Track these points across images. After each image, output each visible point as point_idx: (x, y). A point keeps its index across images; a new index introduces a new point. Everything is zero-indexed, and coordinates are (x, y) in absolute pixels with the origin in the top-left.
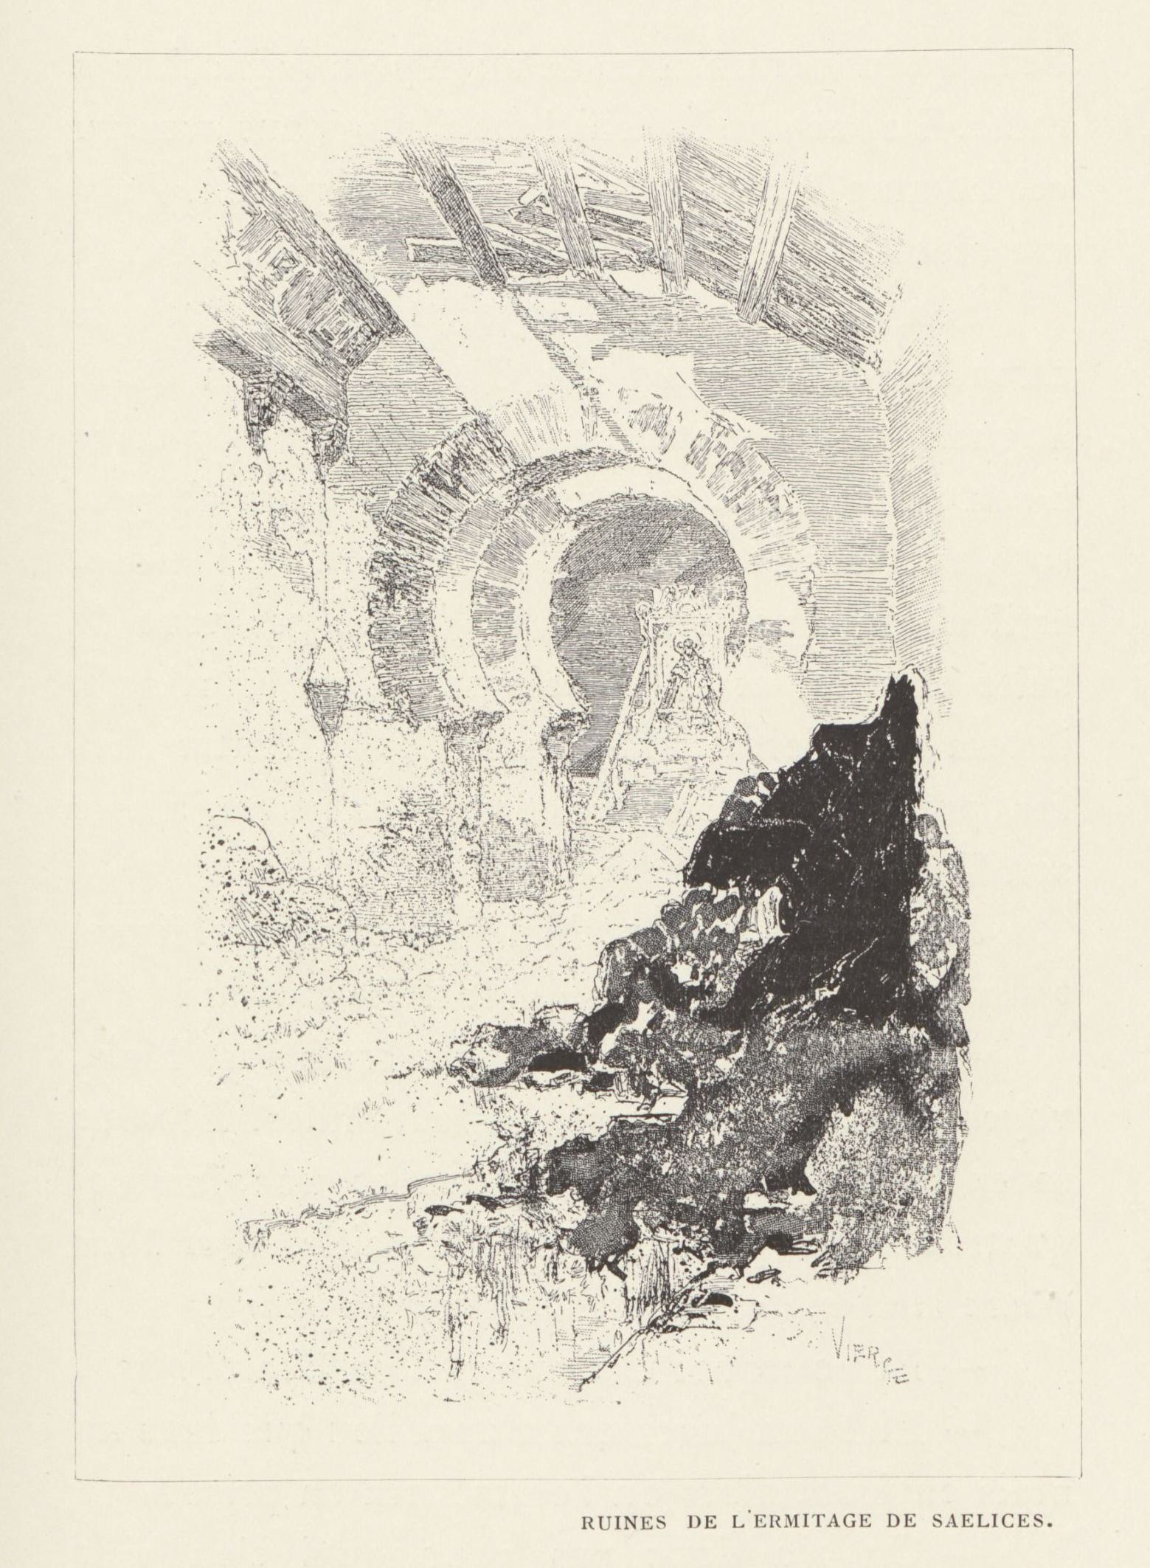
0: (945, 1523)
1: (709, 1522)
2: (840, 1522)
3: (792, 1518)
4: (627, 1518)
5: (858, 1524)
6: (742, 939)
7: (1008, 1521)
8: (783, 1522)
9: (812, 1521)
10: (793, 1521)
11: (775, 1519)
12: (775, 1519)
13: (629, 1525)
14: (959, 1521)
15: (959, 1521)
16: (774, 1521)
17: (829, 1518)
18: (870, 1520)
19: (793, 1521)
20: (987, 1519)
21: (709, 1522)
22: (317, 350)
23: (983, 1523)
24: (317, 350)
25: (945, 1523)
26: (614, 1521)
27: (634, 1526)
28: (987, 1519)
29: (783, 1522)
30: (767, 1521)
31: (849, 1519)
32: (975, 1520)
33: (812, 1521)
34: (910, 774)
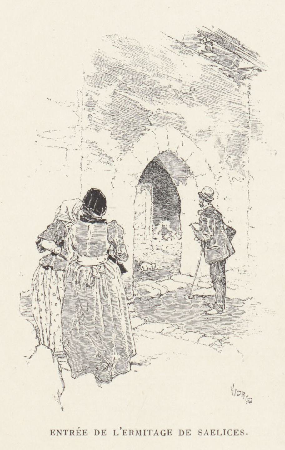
0: (203, 434)
1: (188, 432)
2: (159, 433)
3: (139, 431)
4: (58, 431)
5: (167, 434)
6: (112, 246)
7: (230, 432)
8: (135, 433)
9: (147, 433)
10: (139, 433)
11: (132, 431)
12: (132, 431)
13: (59, 434)
14: (209, 433)
15: (209, 433)
16: (131, 432)
17: (154, 431)
18: (87, 432)
19: (139, 433)
20: (221, 432)
21: (188, 432)
22: (118, 130)
23: (220, 434)
24: (118, 130)
25: (203, 434)
26: (69, 432)
27: (61, 434)
28: (221, 432)
29: (135, 433)
30: (128, 433)
31: (163, 432)
32: (216, 432)
33: (147, 433)
34: (102, 196)
